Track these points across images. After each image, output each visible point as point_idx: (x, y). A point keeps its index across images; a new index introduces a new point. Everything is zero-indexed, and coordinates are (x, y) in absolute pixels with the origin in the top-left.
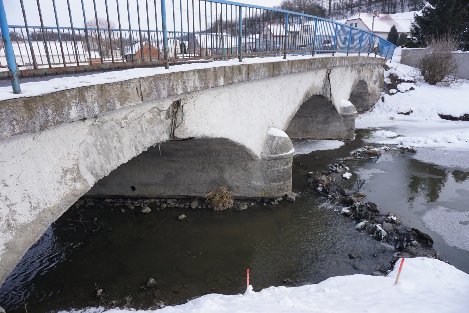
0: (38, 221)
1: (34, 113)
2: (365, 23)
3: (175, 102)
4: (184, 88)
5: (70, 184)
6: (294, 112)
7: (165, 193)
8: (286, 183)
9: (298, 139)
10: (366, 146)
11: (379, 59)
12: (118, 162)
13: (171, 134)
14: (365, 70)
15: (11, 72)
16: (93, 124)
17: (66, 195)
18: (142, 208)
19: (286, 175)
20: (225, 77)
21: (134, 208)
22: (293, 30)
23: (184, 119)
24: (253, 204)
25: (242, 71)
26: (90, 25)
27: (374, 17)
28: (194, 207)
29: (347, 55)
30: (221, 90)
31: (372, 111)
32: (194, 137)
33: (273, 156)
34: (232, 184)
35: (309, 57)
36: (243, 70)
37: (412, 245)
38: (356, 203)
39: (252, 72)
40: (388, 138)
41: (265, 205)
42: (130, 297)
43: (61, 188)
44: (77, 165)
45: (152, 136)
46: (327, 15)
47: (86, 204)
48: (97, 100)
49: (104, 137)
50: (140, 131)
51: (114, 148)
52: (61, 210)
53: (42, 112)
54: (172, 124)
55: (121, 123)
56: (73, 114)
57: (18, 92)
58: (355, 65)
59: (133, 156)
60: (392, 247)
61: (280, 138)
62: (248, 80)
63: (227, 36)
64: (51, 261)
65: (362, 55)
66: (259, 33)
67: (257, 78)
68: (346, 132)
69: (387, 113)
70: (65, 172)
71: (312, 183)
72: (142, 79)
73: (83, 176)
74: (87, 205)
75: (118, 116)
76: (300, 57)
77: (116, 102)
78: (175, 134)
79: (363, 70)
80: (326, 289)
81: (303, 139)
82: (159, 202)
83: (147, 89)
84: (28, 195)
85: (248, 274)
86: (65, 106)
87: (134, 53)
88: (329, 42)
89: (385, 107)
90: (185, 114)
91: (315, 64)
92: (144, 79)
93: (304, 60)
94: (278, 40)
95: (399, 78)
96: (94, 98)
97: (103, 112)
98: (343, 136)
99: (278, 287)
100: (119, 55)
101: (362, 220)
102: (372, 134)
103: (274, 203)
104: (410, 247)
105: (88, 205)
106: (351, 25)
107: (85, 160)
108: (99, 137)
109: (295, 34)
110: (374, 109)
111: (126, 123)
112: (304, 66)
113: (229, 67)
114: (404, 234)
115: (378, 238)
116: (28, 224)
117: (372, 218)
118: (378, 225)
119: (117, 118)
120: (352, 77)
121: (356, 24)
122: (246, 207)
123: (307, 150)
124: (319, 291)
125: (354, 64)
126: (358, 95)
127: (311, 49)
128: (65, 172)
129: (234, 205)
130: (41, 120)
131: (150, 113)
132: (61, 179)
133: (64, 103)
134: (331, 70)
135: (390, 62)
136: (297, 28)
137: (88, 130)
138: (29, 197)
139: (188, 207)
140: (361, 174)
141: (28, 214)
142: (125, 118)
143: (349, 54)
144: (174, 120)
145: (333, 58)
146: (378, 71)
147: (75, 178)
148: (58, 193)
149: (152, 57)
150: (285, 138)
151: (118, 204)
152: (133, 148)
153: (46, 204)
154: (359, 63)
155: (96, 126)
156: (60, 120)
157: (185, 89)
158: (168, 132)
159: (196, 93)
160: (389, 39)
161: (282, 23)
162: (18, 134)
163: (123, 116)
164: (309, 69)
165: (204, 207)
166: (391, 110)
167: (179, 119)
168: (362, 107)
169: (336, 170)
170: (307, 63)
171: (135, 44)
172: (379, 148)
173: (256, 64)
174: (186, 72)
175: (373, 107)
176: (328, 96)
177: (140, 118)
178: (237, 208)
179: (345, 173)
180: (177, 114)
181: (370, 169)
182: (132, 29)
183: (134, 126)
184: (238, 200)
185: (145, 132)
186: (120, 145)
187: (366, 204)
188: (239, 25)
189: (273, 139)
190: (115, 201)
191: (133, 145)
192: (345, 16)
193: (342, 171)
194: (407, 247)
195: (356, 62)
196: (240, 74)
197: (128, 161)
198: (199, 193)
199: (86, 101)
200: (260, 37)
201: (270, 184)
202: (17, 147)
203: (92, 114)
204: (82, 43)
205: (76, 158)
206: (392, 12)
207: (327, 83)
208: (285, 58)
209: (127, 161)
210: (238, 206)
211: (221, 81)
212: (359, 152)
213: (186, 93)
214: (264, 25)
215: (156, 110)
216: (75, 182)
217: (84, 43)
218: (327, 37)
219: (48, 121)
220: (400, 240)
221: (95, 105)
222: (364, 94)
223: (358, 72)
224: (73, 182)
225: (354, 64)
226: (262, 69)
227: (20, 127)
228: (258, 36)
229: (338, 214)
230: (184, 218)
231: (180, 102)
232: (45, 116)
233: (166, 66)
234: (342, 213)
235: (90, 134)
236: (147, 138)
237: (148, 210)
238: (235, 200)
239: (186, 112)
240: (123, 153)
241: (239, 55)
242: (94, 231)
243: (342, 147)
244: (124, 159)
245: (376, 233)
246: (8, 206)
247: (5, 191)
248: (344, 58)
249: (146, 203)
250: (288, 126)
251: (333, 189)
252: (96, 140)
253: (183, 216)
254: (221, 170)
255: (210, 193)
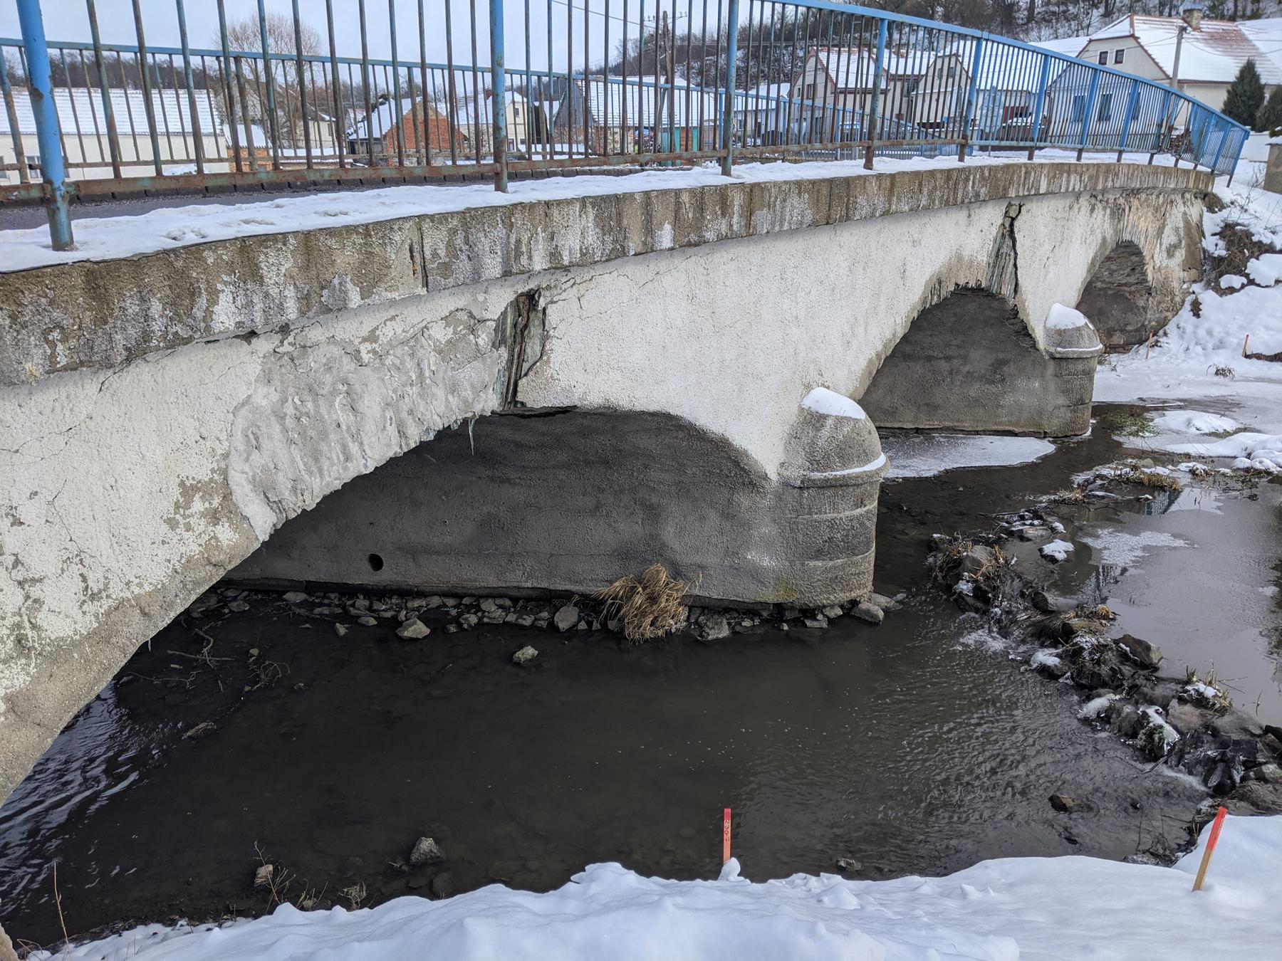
0: (102, 635)
1: (113, 309)
2: (1150, 52)
3: (522, 295)
4: (551, 254)
5: (202, 528)
6: (890, 341)
7: (475, 580)
8: (855, 564)
9: (902, 429)
10: (1129, 460)
11: (1186, 172)
12: (345, 468)
13: (507, 393)
14: (1137, 209)
15: (48, 187)
16: (275, 351)
17: (188, 561)
18: (400, 624)
19: (855, 536)
20: (677, 221)
21: (375, 623)
22: (901, 72)
23: (547, 348)
24: (747, 623)
25: (732, 205)
26: (237, 39)
27: (1183, 29)
28: (563, 626)
29: (1079, 158)
30: (663, 265)
31: (1156, 344)
32: (575, 407)
33: (817, 475)
34: (683, 559)
35: (948, 162)
36: (733, 201)
37: (1262, 778)
38: (1082, 636)
40: (1206, 434)
41: (786, 627)
42: (361, 886)
43: (175, 540)
44: (225, 473)
45: (450, 397)
46: (1020, 22)
47: (223, 607)
48: (292, 277)
49: (306, 392)
50: (414, 378)
51: (334, 425)
52: (171, 605)
53: (133, 308)
54: (510, 361)
55: (359, 351)
56: (223, 318)
57: (67, 245)
58: (1104, 191)
59: (391, 454)
60: (1194, 782)
61: (840, 420)
62: (749, 233)
63: (688, 90)
64: (112, 770)
65: (1128, 158)
66: (790, 78)
67: (777, 228)
68: (1063, 410)
69: (1206, 356)
70: (188, 491)
71: (941, 569)
72: (428, 220)
73: (241, 506)
74: (226, 611)
75: (349, 329)
76: (918, 164)
77: (350, 286)
78: (519, 394)
79: (1130, 208)
80: (969, 888)
81: (917, 430)
82: (454, 607)
83: (442, 253)
84: (77, 555)
85: (727, 824)
86: (200, 293)
87: (376, 134)
88: (1022, 112)
89: (1202, 332)
90: (551, 333)
91: (966, 187)
92: (432, 221)
93: (932, 173)
94: (849, 106)
95: (1255, 239)
96: (284, 271)
97: (311, 314)
98: (1054, 425)
99: (819, 875)
100: (326, 137)
101: (1101, 691)
102: (1152, 420)
103: (816, 624)
104: (1253, 785)
105: (231, 611)
106: (1103, 55)
107: (247, 460)
108: (291, 390)
109: (911, 83)
110: (1163, 339)
111: (374, 352)
112: (931, 193)
113: (692, 191)
114: (1237, 743)
115: (1151, 752)
116: (75, 644)
117: (1134, 688)
118: (1151, 711)
119: (345, 336)
120: (1093, 232)
121: (1119, 54)
122: (724, 632)
123: (927, 465)
124: (947, 894)
125: (1100, 187)
126: (1110, 292)
127: (955, 135)
128: (188, 491)
129: (690, 624)
130: (131, 331)
131: (447, 325)
132: (175, 514)
133: (198, 282)
134: (1020, 207)
135: (1228, 186)
136: (917, 62)
137: (260, 368)
138: (81, 560)
139: (544, 624)
140: (1105, 548)
141: (76, 612)
142: (372, 337)
143: (1084, 155)
144: (517, 350)
145: (1028, 169)
146: (1185, 214)
147: (216, 511)
148: (163, 553)
149: (433, 151)
150: (856, 420)
151: (326, 611)
152: (392, 430)
153: (127, 584)
154: (1117, 185)
155: (286, 358)
156: (184, 333)
157: (554, 255)
158: (498, 387)
159: (586, 269)
160: (1231, 109)
161: (866, 45)
162: (65, 368)
163: (365, 332)
164: (947, 203)
165: (596, 626)
166: (1221, 345)
167: (533, 348)
168: (1121, 331)
169: (1021, 531)
170: (940, 182)
171: (382, 104)
172: (1170, 467)
173: (775, 184)
174: (559, 203)
175: (1161, 332)
176: (1007, 290)
177: (417, 340)
178: (696, 634)
179: (1050, 540)
180: (526, 332)
181: (1136, 533)
182: (370, 57)
183: (397, 362)
184: (702, 608)
185: (428, 381)
186: (352, 418)
187: (1116, 642)
188: (728, 50)
189: (818, 422)
190: (317, 601)
191: (391, 419)
192: (1084, 25)
193: (1042, 536)
194: (1244, 784)
195: (1106, 181)
196: (723, 215)
197: (376, 468)
198: (581, 583)
199: (261, 281)
200: (790, 94)
201: (803, 564)
202: (53, 411)
203: (277, 321)
204: (209, 98)
205: (220, 452)
206: (1248, 13)
207: (1005, 250)
208: (868, 165)
209: (371, 469)
210: (700, 627)
211: (666, 237)
212: (1102, 477)
213: (556, 268)
214: (807, 53)
215: (463, 316)
216: (215, 525)
217: (216, 95)
218: (1014, 94)
219: (148, 335)
220: (1221, 760)
221: (286, 293)
222: (1133, 289)
223: (1113, 214)
224: (209, 523)
225: (1100, 187)
226: (794, 200)
227: (70, 349)
228: (785, 88)
229: (1022, 669)
230: (532, 659)
231: (536, 296)
232: (143, 320)
233: (496, 179)
234: (1035, 666)
235: (266, 381)
236: (434, 402)
237: (418, 629)
238: (691, 608)
239: (555, 328)
240: (361, 443)
241: (723, 153)
242: (247, 688)
243: (1045, 459)
244: (364, 461)
245: (1144, 734)
246: (20, 583)
247: (13, 539)
248: (1066, 168)
249: (413, 610)
250: (868, 383)
251: (1007, 589)
252: (284, 401)
253: (529, 652)
254: (653, 513)
255: (617, 584)
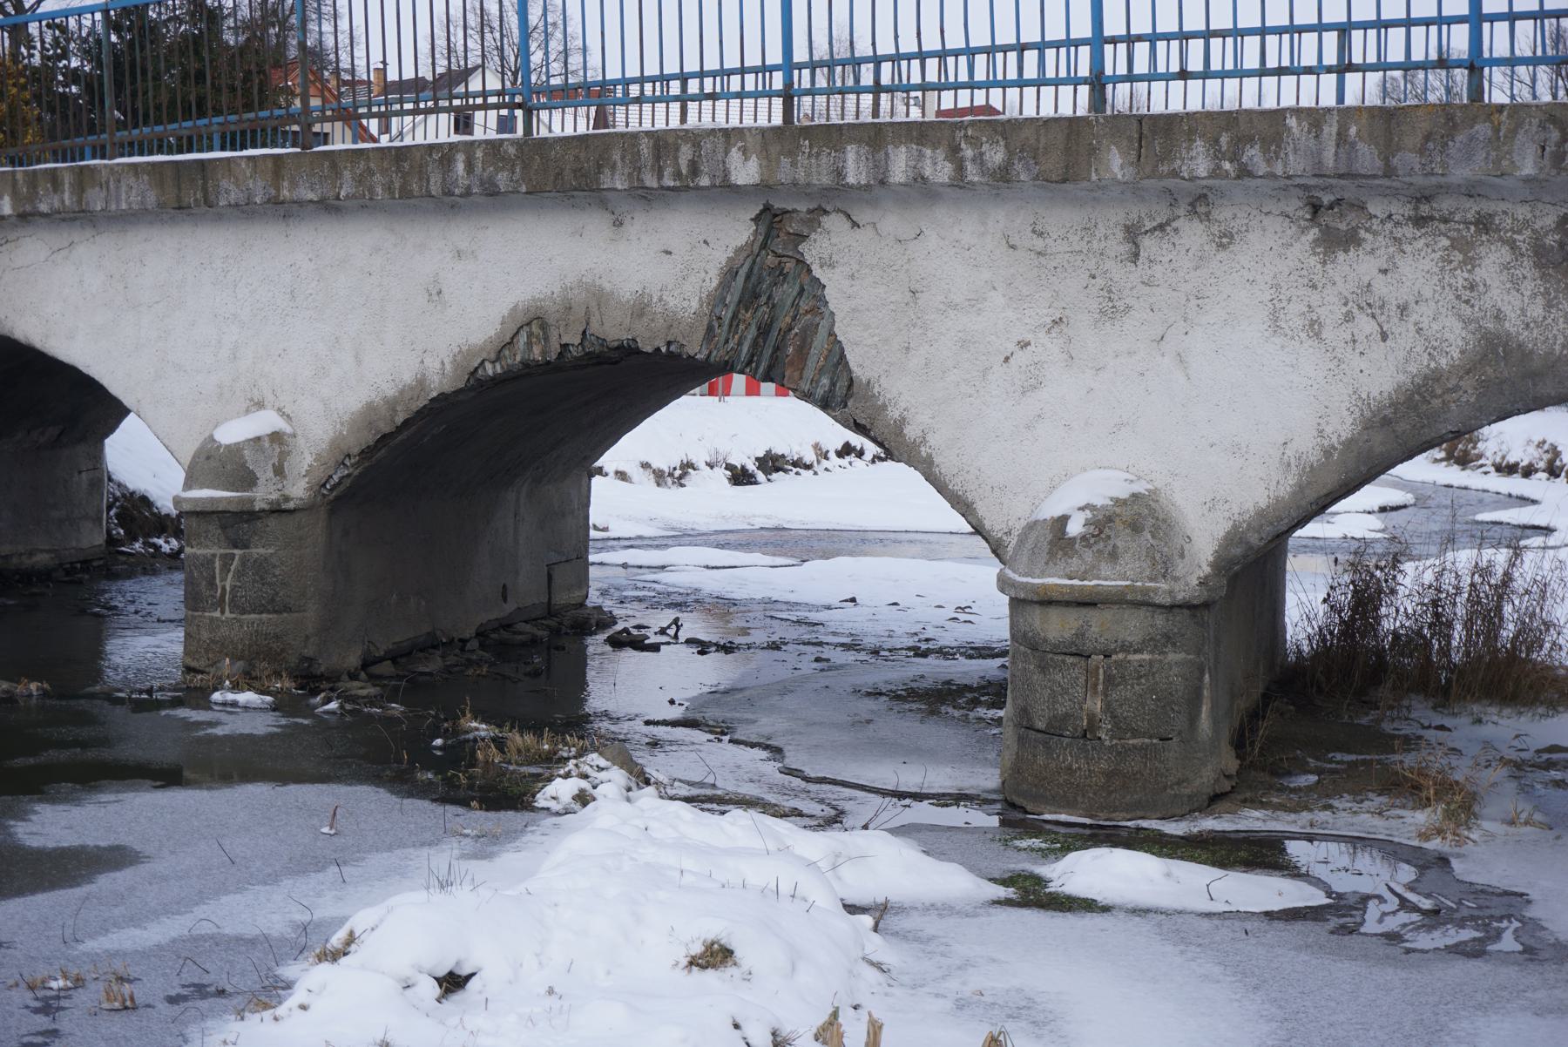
36: (63, 180)
39: (93, 187)
164: (406, 194)
